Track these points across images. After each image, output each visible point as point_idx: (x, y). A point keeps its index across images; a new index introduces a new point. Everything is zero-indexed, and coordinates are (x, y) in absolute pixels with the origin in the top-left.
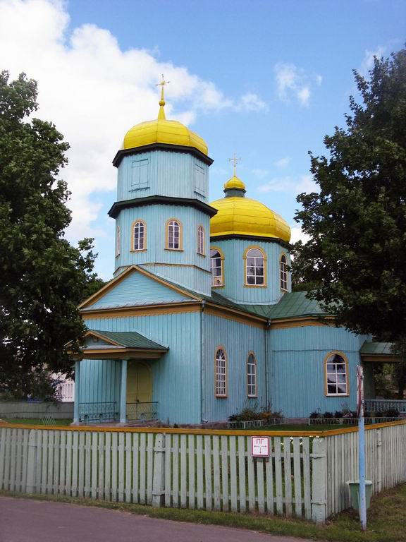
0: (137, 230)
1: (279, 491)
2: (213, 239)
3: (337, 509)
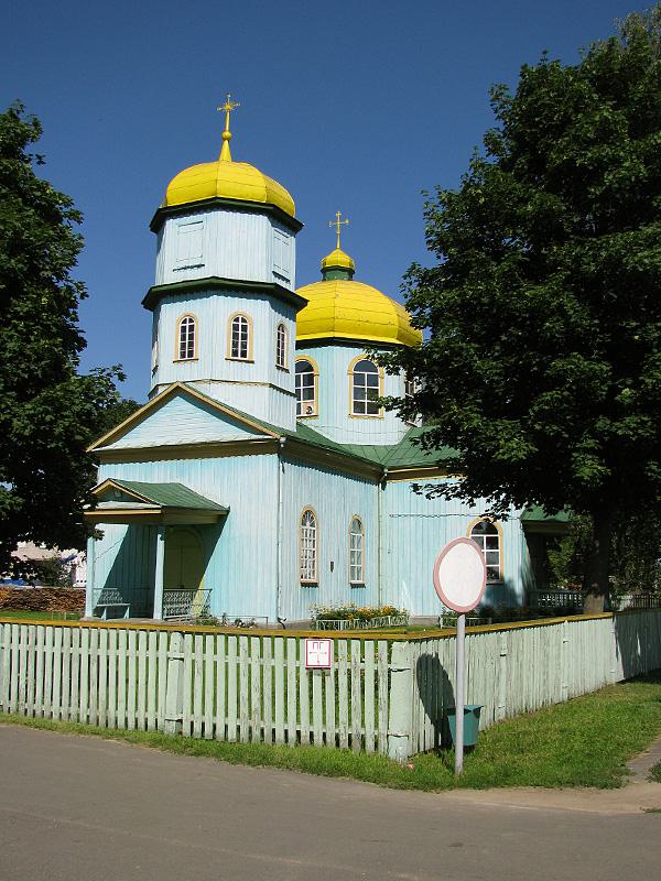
0: (184, 329)
1: (343, 717)
2: (301, 345)
3: (428, 744)
